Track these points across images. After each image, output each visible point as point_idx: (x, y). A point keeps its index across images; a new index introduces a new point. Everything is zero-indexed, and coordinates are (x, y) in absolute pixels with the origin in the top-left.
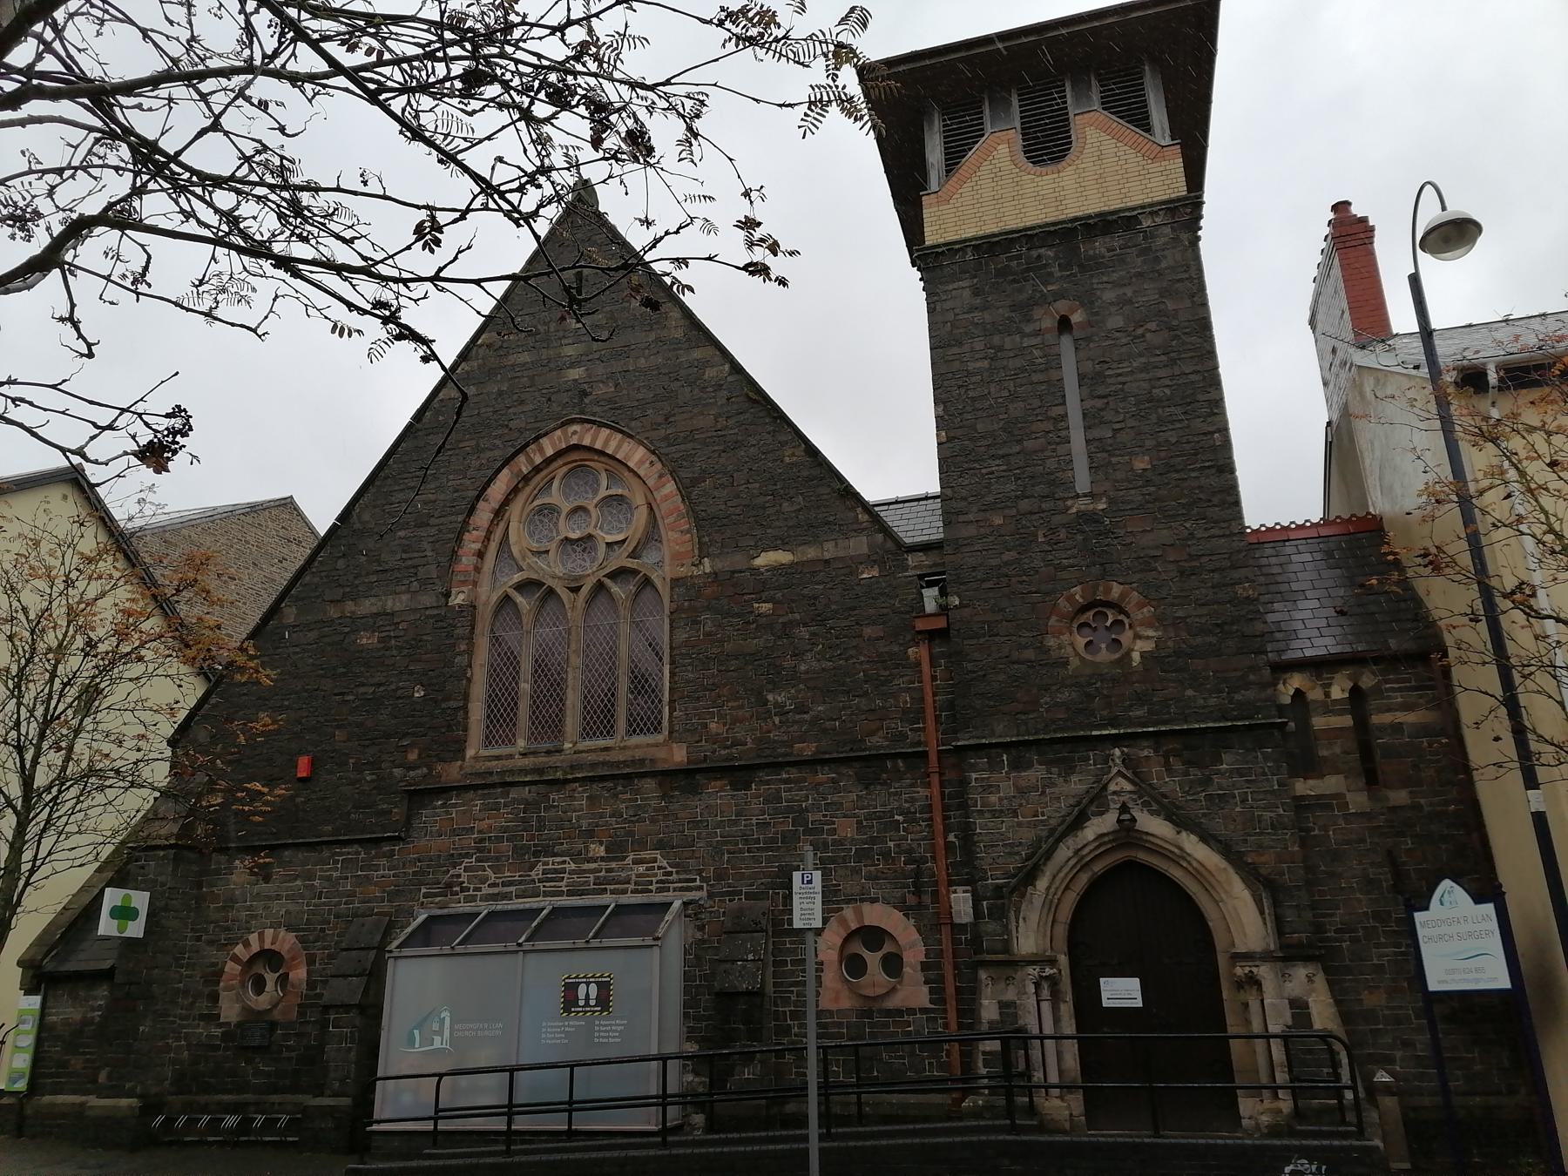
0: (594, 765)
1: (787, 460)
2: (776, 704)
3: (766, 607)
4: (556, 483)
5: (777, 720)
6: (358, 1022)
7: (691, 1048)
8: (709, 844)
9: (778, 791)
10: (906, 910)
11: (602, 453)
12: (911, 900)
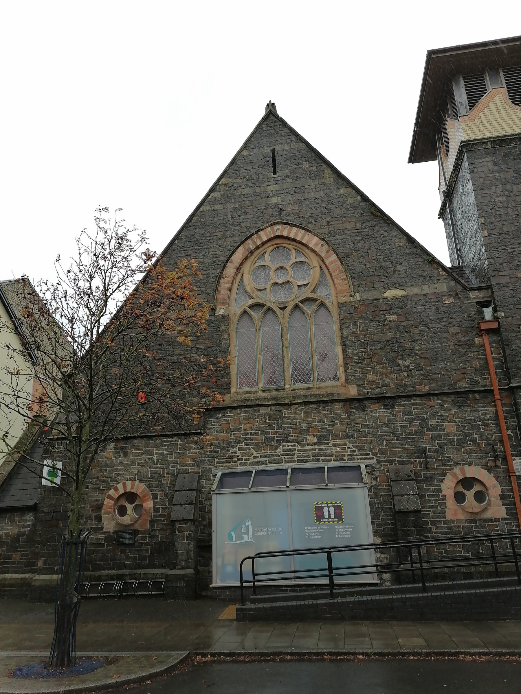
0: (305, 396)
1: (397, 244)
2: (404, 366)
3: (393, 318)
4: (267, 255)
5: (405, 374)
6: (193, 528)
7: (379, 540)
8: (374, 436)
9: (410, 409)
10: (489, 469)
11: (294, 240)
12: (491, 464)
